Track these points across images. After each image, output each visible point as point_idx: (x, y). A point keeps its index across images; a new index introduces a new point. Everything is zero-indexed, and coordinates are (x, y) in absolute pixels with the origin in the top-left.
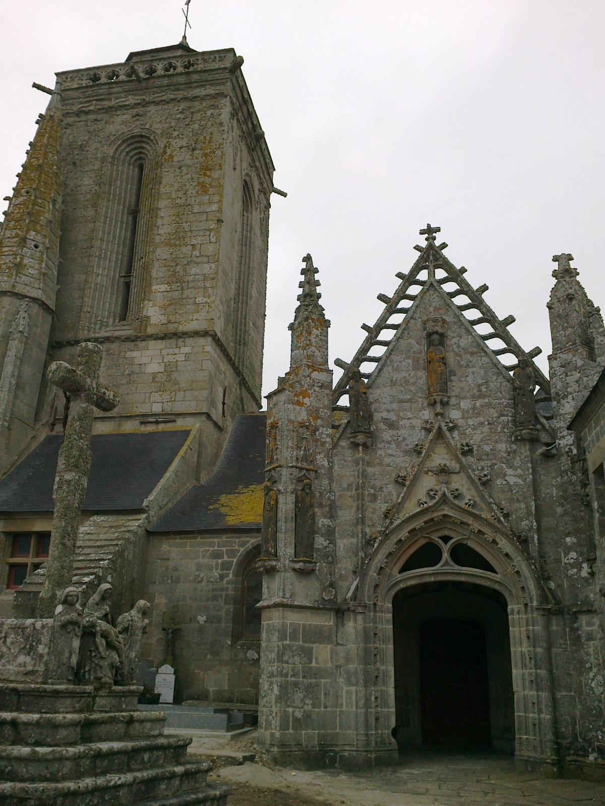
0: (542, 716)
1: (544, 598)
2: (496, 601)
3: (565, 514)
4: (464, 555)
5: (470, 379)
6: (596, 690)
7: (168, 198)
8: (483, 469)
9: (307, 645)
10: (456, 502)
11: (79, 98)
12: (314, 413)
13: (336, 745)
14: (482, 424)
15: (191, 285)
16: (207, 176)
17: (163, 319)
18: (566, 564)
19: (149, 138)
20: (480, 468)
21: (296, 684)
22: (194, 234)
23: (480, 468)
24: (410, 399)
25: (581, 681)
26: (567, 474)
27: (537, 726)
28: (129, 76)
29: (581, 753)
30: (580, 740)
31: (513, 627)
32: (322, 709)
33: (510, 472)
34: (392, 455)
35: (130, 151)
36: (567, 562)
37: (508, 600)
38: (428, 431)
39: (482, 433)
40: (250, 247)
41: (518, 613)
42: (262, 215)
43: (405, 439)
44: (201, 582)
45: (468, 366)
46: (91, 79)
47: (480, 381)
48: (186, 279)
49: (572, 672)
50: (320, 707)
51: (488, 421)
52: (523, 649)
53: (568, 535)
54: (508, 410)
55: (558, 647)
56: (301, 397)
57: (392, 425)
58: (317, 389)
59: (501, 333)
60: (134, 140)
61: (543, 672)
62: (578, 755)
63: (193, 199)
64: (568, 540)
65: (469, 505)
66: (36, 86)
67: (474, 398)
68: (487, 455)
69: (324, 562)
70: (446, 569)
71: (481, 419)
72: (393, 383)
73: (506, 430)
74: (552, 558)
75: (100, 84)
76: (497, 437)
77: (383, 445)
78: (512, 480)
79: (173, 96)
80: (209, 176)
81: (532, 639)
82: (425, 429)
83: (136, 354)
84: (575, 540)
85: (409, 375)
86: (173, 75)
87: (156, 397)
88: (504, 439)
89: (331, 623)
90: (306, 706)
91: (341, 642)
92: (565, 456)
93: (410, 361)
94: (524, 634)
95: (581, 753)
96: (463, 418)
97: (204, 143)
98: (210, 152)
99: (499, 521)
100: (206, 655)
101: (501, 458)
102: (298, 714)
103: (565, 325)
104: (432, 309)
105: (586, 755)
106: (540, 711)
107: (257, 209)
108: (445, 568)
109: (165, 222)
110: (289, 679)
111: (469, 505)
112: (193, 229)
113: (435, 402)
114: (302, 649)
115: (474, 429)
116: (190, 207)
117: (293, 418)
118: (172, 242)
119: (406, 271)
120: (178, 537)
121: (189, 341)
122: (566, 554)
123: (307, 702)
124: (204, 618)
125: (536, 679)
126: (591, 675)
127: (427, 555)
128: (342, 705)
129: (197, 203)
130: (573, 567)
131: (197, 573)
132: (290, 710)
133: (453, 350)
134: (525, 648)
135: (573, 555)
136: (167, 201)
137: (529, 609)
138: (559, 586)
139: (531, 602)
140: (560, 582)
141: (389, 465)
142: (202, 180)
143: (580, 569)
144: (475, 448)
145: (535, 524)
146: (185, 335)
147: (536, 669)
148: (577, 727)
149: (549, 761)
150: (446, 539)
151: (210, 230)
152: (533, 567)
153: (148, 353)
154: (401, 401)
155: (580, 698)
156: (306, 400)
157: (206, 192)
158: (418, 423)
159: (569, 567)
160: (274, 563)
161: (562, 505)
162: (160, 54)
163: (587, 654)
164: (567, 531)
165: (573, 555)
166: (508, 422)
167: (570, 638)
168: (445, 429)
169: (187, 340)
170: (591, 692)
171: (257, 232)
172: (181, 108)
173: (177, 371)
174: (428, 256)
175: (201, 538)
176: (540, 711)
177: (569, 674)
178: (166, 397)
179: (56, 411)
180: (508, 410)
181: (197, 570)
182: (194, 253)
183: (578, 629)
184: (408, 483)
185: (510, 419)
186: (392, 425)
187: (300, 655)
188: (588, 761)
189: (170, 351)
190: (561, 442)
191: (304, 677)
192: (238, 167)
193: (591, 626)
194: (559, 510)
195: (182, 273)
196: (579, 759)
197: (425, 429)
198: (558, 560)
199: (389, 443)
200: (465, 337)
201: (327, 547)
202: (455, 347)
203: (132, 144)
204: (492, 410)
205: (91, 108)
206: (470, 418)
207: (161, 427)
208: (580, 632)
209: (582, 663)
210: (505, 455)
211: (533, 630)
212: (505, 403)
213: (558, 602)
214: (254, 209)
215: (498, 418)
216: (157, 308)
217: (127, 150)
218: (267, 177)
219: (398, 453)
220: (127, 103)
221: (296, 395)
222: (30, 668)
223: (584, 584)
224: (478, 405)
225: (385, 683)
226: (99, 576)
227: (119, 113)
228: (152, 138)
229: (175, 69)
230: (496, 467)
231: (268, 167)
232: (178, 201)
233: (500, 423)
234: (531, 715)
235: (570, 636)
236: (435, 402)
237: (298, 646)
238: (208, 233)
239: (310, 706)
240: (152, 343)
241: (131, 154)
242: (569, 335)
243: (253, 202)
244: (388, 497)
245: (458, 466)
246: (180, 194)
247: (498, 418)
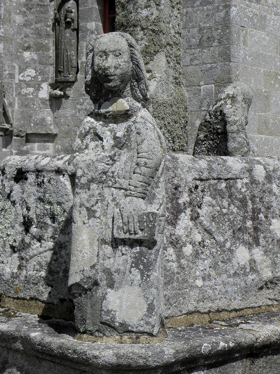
3: (26, 24)
18: (20, 80)
36: (22, 79)
53: (28, 48)
64: (27, 55)
74: (7, 72)
84: (35, 57)
122: (21, 70)
130: (28, 85)
135: (31, 72)
140: (12, 100)
143: (38, 88)
159: (23, 85)
161: (24, 14)
164: (26, 45)
165: (31, 72)
193: (45, 150)
194: (19, 19)
198: (12, 76)
223: (41, 106)
225: (49, 49)
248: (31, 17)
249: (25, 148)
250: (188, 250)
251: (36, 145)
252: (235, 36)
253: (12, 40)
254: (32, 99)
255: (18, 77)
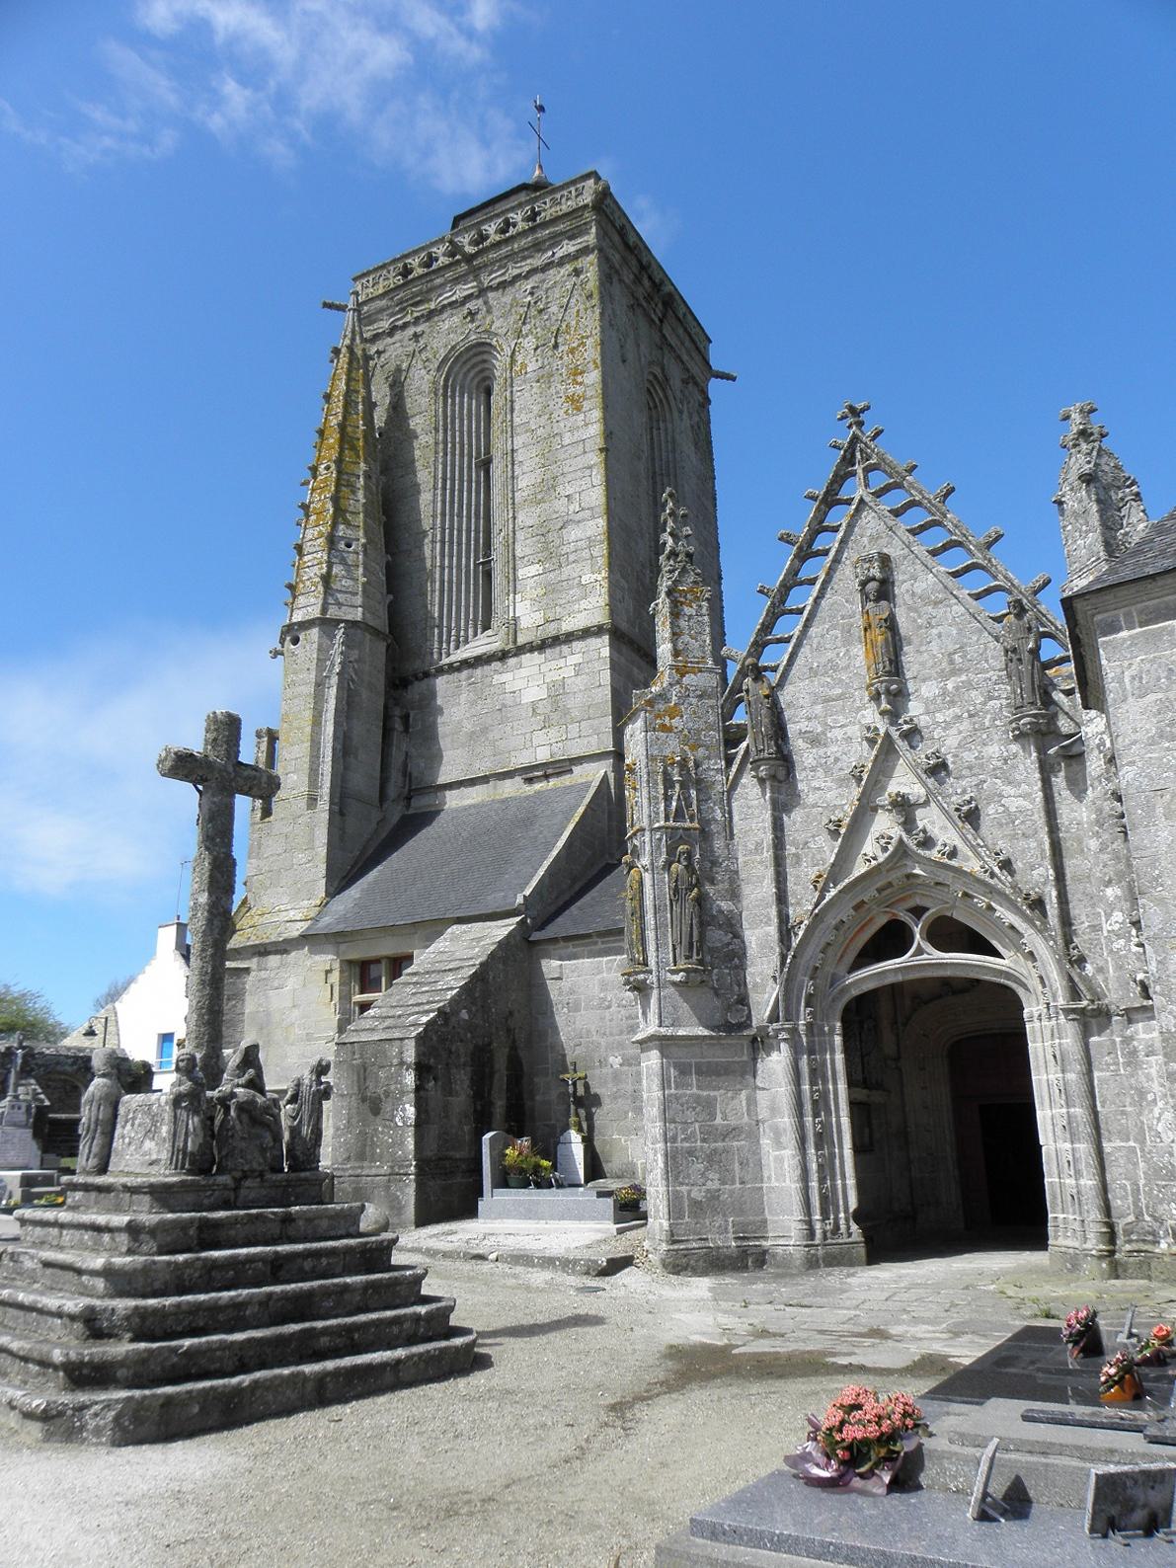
0: (1082, 1182)
1: (1074, 993)
2: (1003, 1001)
4: (953, 934)
5: (934, 647)
6: (1163, 1135)
7: (527, 431)
8: (964, 792)
9: (705, 1093)
10: (926, 853)
11: (388, 308)
12: (692, 740)
13: (765, 1238)
14: (958, 717)
15: (572, 558)
16: (577, 383)
17: (539, 618)
18: (1109, 931)
19: (490, 344)
20: (959, 791)
21: (691, 1152)
22: (569, 477)
23: (959, 791)
24: (842, 694)
25: (1142, 1123)
26: (1100, 782)
27: (1077, 1198)
28: (452, 254)
29: (1150, 1238)
30: (1147, 1218)
31: (1034, 1042)
32: (738, 1185)
33: (1009, 790)
34: (819, 789)
35: (469, 371)
36: (1110, 928)
37: (1023, 1000)
38: (872, 742)
39: (960, 732)
40: (675, 476)
41: (1040, 1018)
42: (696, 419)
43: (837, 760)
44: (609, 1007)
45: (930, 626)
46: (400, 274)
47: (951, 648)
48: (565, 549)
49: (1129, 1109)
50: (733, 1183)
51: (968, 711)
52: (1051, 1077)
53: (1109, 883)
54: (1000, 689)
55: (1102, 1070)
56: (667, 718)
57: (815, 741)
58: (694, 701)
59: (980, 561)
60: (471, 353)
61: (1079, 1111)
62: (1144, 1241)
63: (562, 425)
64: (1109, 892)
65: (943, 854)
66: (326, 305)
67: (944, 676)
68: (970, 768)
69: (726, 967)
70: (925, 957)
71: (957, 711)
72: (813, 673)
73: (998, 723)
75: (440, 269)
76: (985, 736)
77: (804, 774)
78: (1014, 804)
79: (516, 272)
80: (581, 384)
81: (1061, 1060)
82: (868, 739)
83: (507, 677)
85: (838, 654)
86: (512, 237)
87: (540, 737)
88: (996, 737)
89: (745, 1058)
90: (709, 1182)
91: (760, 1085)
92: (1096, 752)
93: (838, 633)
94: (1049, 1051)
95: (1150, 1238)
96: (927, 713)
97: (569, 333)
98: (579, 346)
99: (993, 875)
100: (626, 1113)
101: (994, 770)
102: (698, 1194)
103: (1084, 528)
104: (865, 540)
105: (1156, 1243)
106: (1078, 1174)
107: (681, 412)
108: (919, 958)
109: (525, 469)
110: (678, 1145)
111: (943, 854)
112: (565, 471)
113: (879, 694)
114: (698, 1099)
115: (945, 729)
116: (558, 438)
117: (656, 752)
118: (539, 497)
119: (820, 492)
120: (570, 944)
121: (577, 645)
122: (1108, 916)
123: (710, 1177)
124: (619, 1060)
125: (1069, 1123)
126: (1157, 1111)
127: (891, 940)
128: (769, 1178)
129: (567, 429)
130: (1119, 937)
131: (602, 995)
132: (684, 1189)
133: (905, 604)
134: (1054, 1075)
136: (524, 436)
137: (1052, 1010)
138: (1100, 970)
139: (1055, 1000)
141: (815, 806)
142: (570, 392)
144: (950, 760)
145: (1051, 872)
146: (570, 638)
147: (1068, 1106)
148: (1142, 1197)
149: (1094, 1252)
150: (918, 912)
151: (590, 467)
152: (1051, 943)
153: (524, 672)
154: (827, 700)
155: (1142, 1151)
156: (676, 722)
157: (579, 409)
158: (855, 731)
159: (1114, 938)
160: (641, 977)
161: (1097, 835)
162: (497, 206)
163: (1149, 1078)
164: (1107, 878)
166: (1001, 708)
167: (1123, 1054)
168: (895, 735)
169: (574, 644)
170: (1158, 1140)
171: (687, 447)
172: (529, 287)
173: (564, 693)
174: (853, 455)
175: (603, 943)
176: (1078, 1174)
177: (1123, 1113)
178: (553, 733)
179: (410, 780)
180: (1000, 689)
181: (602, 990)
182: (571, 508)
183: (1132, 1038)
184: (843, 831)
185: (1004, 702)
186: (815, 741)
187: (694, 1109)
188: (1157, 1251)
189: (553, 664)
190: (1088, 730)
191: (704, 1140)
192: (630, 356)
195: (558, 542)
196: (1145, 1247)
197: (868, 739)
198: (1096, 928)
199: (813, 769)
200: (921, 576)
201: (729, 944)
202: (907, 597)
203: (469, 359)
204: (974, 693)
205: (408, 318)
206: (939, 711)
207: (553, 782)
208: (1135, 1043)
209: (1142, 1093)
210: (999, 764)
211: (1060, 1044)
212: (995, 677)
213: (1097, 996)
214: (676, 414)
215: (984, 704)
216: (528, 602)
217: (465, 369)
218: (697, 358)
219: (829, 784)
220: (454, 299)
221: (658, 716)
222: (154, 1157)
224: (950, 686)
226: (446, 1013)
227: (445, 316)
228: (494, 343)
229: (514, 227)
230: (985, 786)
231: (697, 341)
232: (540, 432)
233: (987, 712)
234: (1068, 1181)
235: (1122, 1050)
236: (879, 694)
237: (691, 1096)
238: (588, 472)
239: (716, 1182)
240: (526, 658)
241: (472, 374)
242: (1090, 545)
243: (673, 403)
244: (818, 857)
245: (923, 791)
246: (543, 420)
247: (984, 704)
248: (1106, 836)
249: (1128, 1032)
250: (127, 1140)
251: (1140, 1025)
252: (1140, 812)
253: (1088, 877)
254: (1125, 956)
255: (1106, 927)
